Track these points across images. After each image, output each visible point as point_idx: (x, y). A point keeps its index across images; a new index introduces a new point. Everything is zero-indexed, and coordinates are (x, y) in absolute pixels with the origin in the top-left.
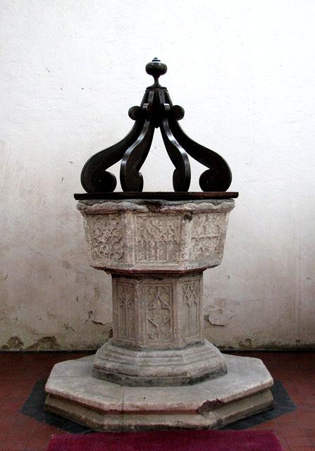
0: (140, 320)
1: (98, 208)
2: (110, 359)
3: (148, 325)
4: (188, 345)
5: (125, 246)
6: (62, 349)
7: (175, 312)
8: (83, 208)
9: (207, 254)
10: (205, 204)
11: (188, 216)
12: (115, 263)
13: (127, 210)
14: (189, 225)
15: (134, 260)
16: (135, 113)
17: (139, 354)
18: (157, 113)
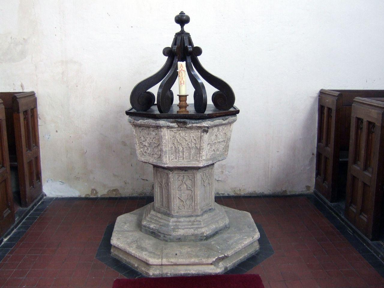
0: (172, 197)
1: (142, 123)
2: (153, 222)
3: (178, 200)
4: (204, 212)
5: (161, 150)
6: (123, 196)
7: (196, 192)
8: (132, 122)
9: (218, 153)
10: (217, 121)
11: (205, 130)
12: (155, 161)
13: (163, 126)
14: (206, 136)
15: (168, 160)
16: (167, 52)
17: (172, 220)
18: (183, 50)
